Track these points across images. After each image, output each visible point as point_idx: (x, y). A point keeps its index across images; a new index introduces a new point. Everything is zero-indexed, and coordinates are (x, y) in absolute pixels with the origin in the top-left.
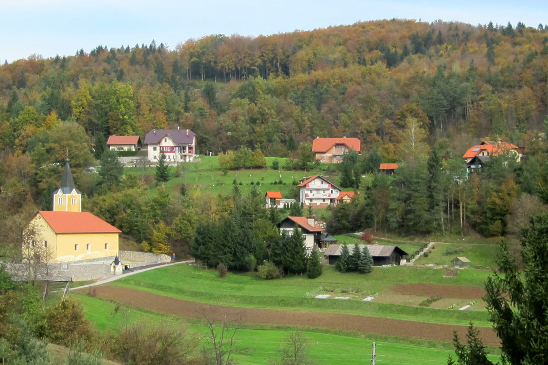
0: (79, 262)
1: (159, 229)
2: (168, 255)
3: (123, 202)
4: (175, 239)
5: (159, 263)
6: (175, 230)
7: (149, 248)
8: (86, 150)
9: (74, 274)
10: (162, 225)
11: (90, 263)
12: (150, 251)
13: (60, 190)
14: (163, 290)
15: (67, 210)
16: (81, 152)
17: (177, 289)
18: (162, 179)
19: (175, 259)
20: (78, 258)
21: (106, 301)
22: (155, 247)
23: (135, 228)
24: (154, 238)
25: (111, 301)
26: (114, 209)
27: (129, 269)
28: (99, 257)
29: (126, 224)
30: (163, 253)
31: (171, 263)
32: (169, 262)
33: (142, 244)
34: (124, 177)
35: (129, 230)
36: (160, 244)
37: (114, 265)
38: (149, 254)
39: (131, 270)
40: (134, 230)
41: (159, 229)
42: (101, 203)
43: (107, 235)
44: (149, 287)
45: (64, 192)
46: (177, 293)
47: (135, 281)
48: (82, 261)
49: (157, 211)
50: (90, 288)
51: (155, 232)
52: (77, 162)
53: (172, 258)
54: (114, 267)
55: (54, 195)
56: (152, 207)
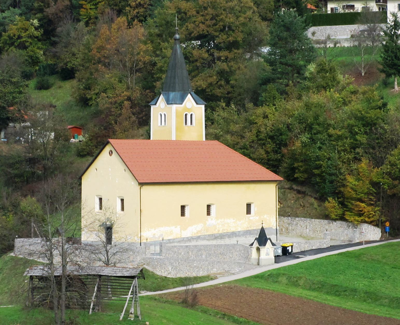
0: (190, 239)
1: (358, 176)
2: (377, 225)
3: (301, 120)
4: (389, 192)
5: (358, 241)
6: (389, 174)
7: (340, 212)
8: (249, 13)
9: (172, 264)
10: (364, 165)
11: (214, 242)
12: (342, 218)
13: (161, 96)
14: (339, 295)
15: (174, 138)
16: (238, 17)
17: (366, 293)
18: (393, 71)
19: (390, 234)
20: (187, 233)
21: (215, 316)
22: (350, 210)
23: (316, 171)
24: (348, 191)
25: (224, 315)
26: (281, 134)
27: (290, 254)
28: (233, 230)
29: (300, 164)
30: (366, 222)
31: (381, 241)
32: (378, 239)
33: (327, 204)
34: (312, 67)
35: (306, 176)
36: (358, 203)
37: (258, 245)
38: (339, 223)
39: (295, 256)
40: (315, 175)
41: (358, 176)
42: (260, 121)
43: (252, 186)
44: (314, 290)
45: (168, 102)
46: (365, 301)
47: (289, 278)
48: (198, 238)
49: (358, 137)
50: (187, 291)
51: (351, 180)
52: (231, 39)
53: (384, 231)
54: (258, 249)
55: (152, 107)
56: (350, 128)
